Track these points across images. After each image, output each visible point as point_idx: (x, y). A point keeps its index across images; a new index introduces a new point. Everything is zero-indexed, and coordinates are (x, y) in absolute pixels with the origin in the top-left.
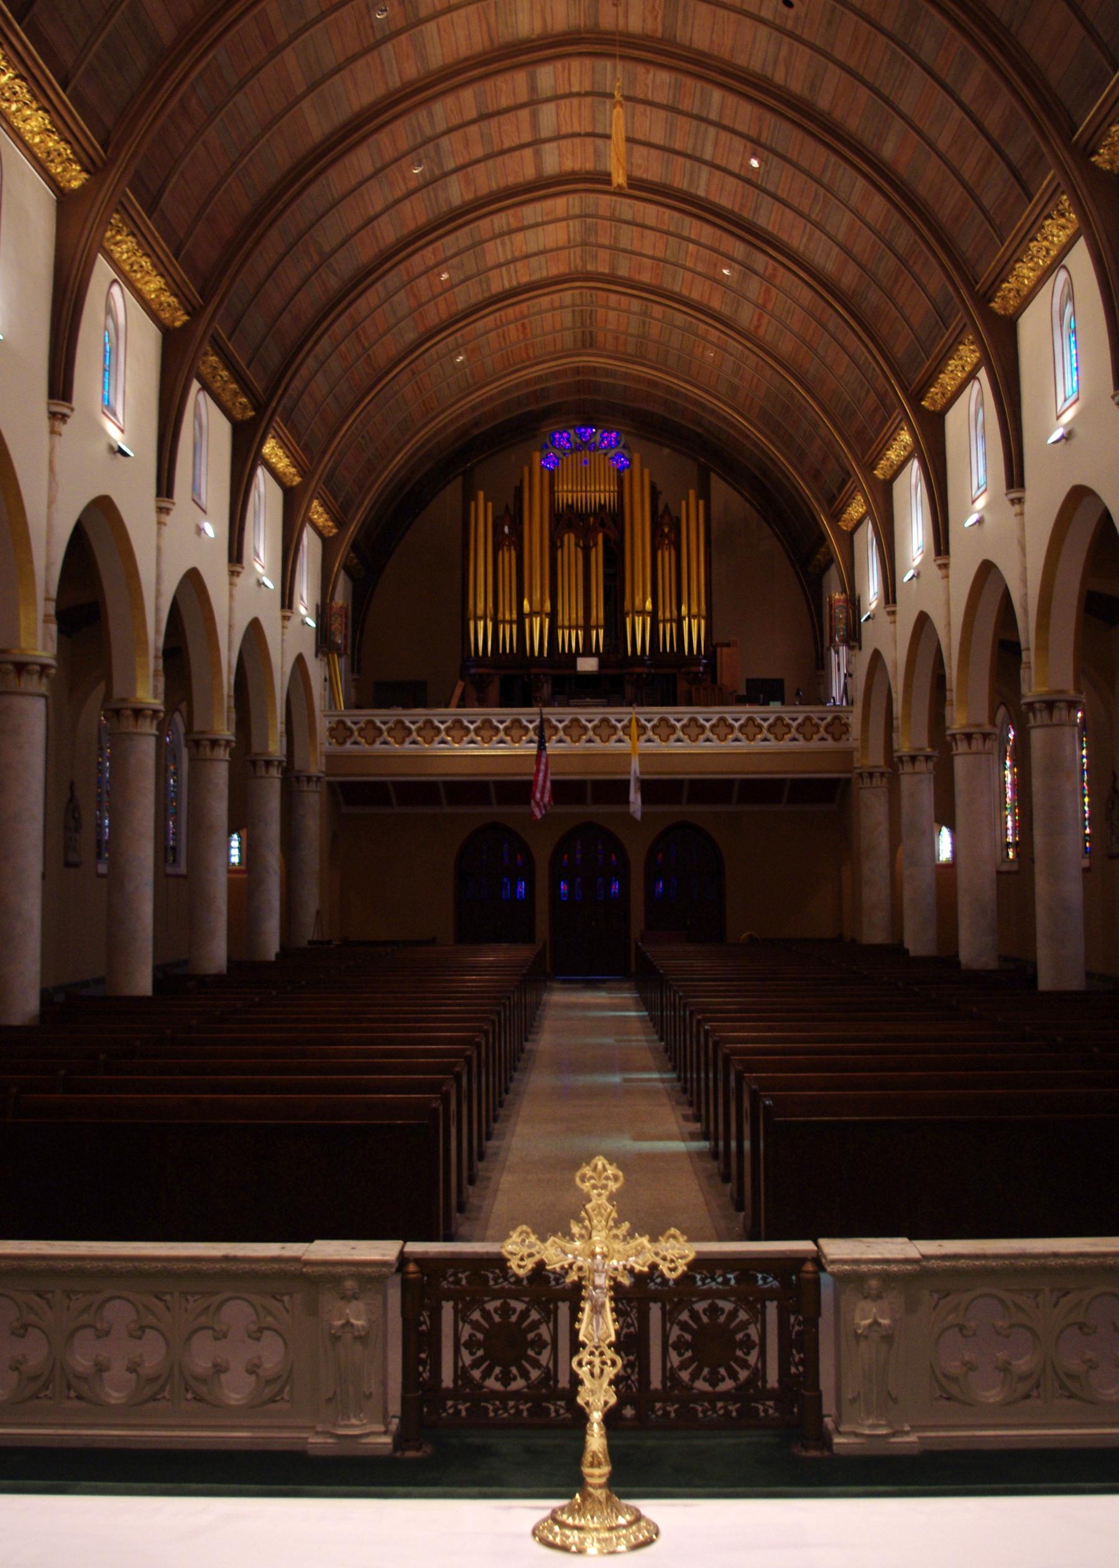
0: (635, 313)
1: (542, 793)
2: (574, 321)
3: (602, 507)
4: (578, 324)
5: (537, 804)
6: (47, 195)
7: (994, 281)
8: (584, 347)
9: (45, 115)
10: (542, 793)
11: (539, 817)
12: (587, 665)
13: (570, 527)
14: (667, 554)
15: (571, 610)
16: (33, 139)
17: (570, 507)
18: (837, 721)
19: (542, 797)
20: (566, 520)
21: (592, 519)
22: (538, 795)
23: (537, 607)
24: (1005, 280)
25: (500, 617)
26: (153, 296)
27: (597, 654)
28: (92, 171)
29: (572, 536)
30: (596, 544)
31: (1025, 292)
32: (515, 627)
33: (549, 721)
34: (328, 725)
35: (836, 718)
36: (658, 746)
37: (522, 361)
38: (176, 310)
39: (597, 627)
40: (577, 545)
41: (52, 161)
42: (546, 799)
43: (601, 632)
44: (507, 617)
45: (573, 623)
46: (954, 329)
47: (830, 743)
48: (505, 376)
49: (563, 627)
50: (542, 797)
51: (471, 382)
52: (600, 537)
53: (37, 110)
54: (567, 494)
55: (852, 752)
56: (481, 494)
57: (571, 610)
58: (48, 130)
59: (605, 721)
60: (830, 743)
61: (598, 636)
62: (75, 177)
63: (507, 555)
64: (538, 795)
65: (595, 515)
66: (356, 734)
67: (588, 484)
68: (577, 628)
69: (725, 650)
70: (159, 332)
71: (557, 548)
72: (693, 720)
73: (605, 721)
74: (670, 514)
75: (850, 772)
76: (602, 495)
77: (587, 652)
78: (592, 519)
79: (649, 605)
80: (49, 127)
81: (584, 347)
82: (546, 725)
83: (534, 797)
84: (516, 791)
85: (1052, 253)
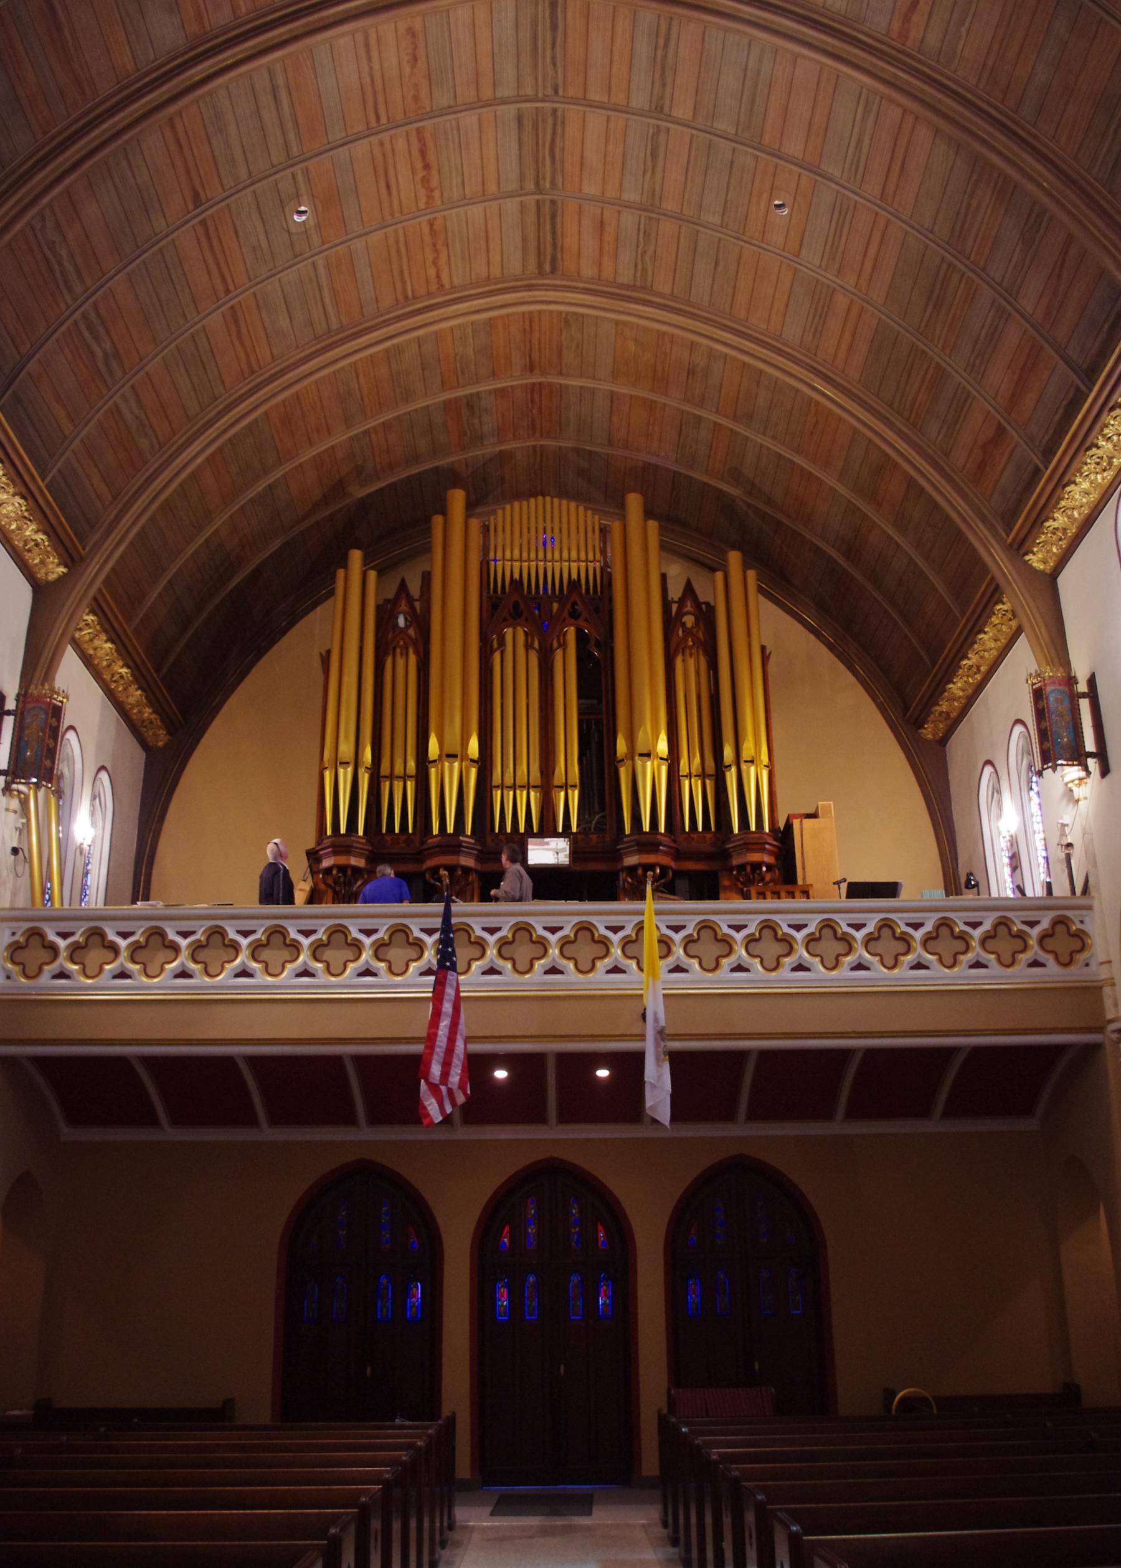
0: (629, 206)
1: (446, 1065)
2: (522, 178)
3: (574, 585)
4: (530, 185)
5: (434, 1089)
6: (25, 593)
7: (954, 658)
8: (541, 273)
9: (22, 501)
10: (446, 1065)
11: (438, 1118)
12: (547, 853)
13: (516, 615)
14: (691, 662)
15: (518, 761)
16: (10, 525)
17: (517, 584)
18: (1060, 928)
19: (445, 1075)
20: (508, 606)
21: (555, 606)
22: (436, 1070)
23: (454, 746)
24: (965, 657)
25: (385, 769)
26: (13, 527)
27: (566, 833)
28: (70, 564)
29: (520, 632)
30: (563, 645)
31: (954, 715)
32: (410, 785)
33: (466, 929)
34: (7, 939)
35: (1060, 922)
36: (697, 980)
37: (430, 294)
38: (159, 728)
39: (565, 787)
40: (528, 646)
41: (29, 551)
42: (455, 1079)
43: (575, 796)
44: (399, 770)
45: (522, 778)
46: (973, 612)
47: (1052, 971)
48: (400, 318)
49: (502, 787)
50: (445, 1075)
51: (335, 325)
52: (571, 633)
53: (14, 495)
54: (514, 561)
55: (1101, 988)
56: (356, 556)
57: (518, 761)
58: (25, 517)
59: (585, 928)
60: (1052, 971)
61: (569, 802)
62: (161, 738)
63: (401, 662)
64: (436, 1070)
65: (561, 598)
66: (64, 954)
67: (547, 542)
68: (528, 787)
69: (808, 823)
70: (30, 588)
71: (492, 652)
72: (768, 926)
73: (585, 928)
74: (695, 598)
75: (1100, 1030)
76: (574, 565)
77: (547, 830)
78: (555, 606)
79: (662, 747)
80: (26, 514)
81: (541, 273)
82: (459, 939)
83: (426, 1075)
84: (389, 1080)
85: (983, 669)
